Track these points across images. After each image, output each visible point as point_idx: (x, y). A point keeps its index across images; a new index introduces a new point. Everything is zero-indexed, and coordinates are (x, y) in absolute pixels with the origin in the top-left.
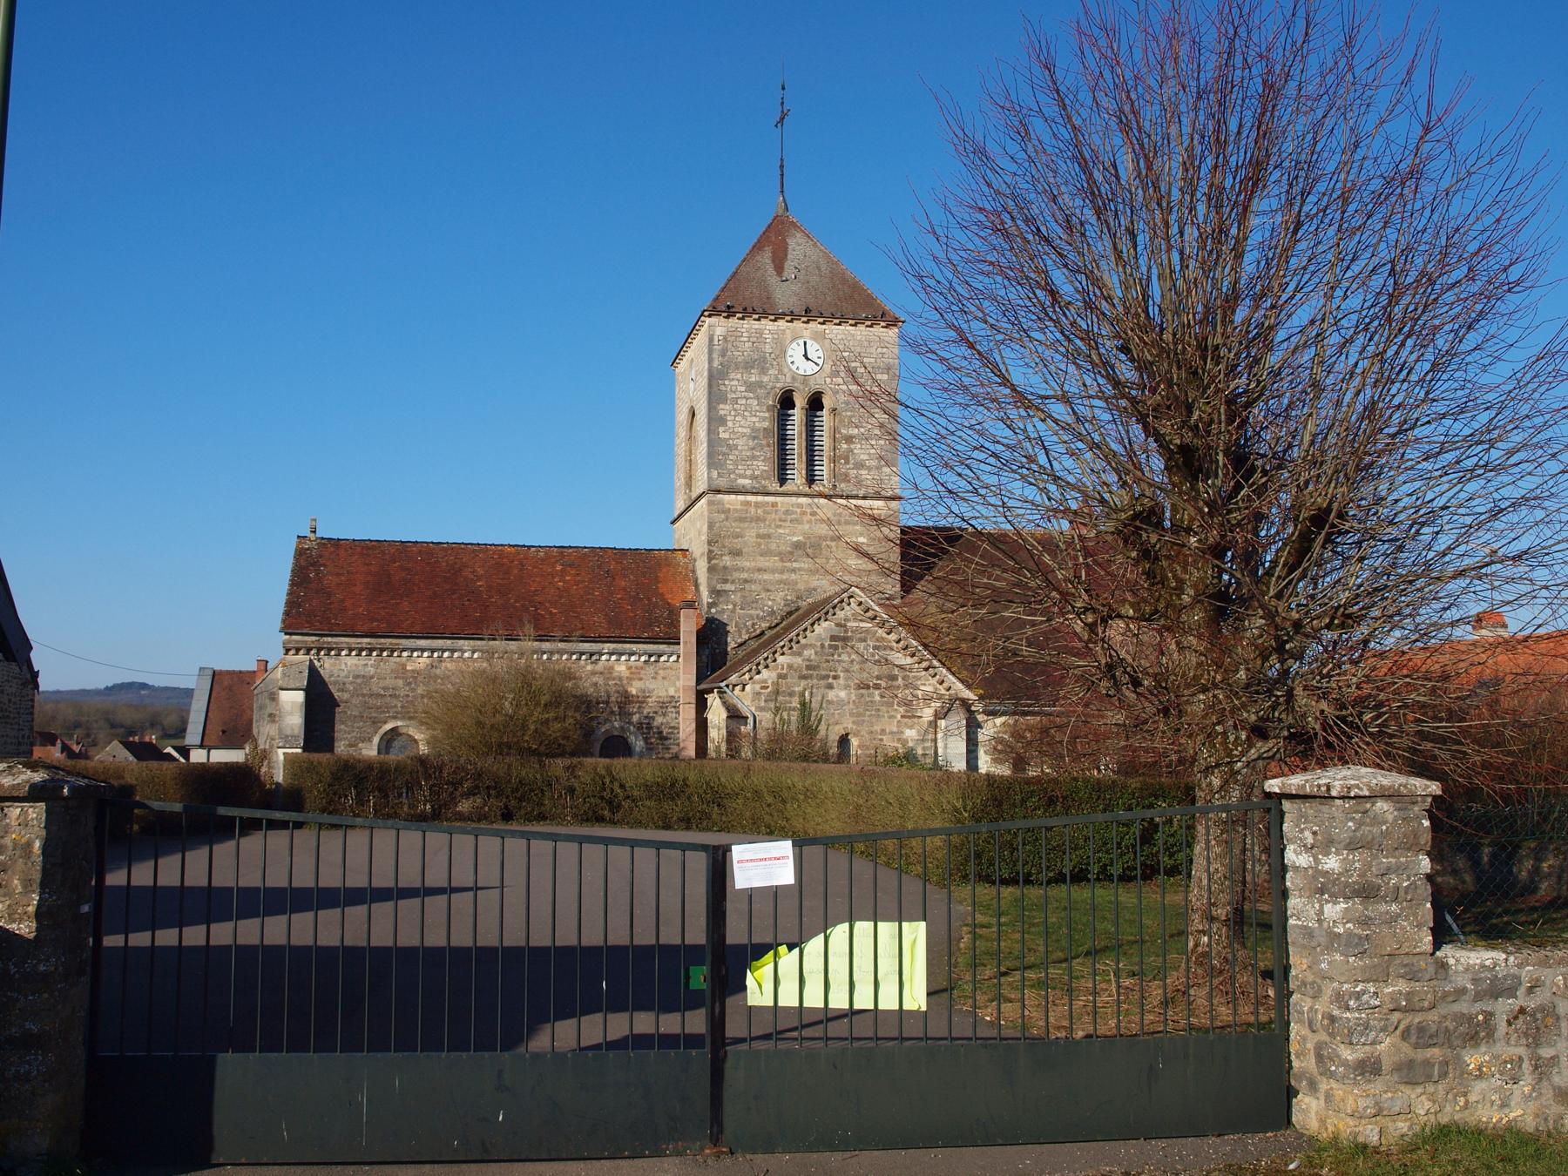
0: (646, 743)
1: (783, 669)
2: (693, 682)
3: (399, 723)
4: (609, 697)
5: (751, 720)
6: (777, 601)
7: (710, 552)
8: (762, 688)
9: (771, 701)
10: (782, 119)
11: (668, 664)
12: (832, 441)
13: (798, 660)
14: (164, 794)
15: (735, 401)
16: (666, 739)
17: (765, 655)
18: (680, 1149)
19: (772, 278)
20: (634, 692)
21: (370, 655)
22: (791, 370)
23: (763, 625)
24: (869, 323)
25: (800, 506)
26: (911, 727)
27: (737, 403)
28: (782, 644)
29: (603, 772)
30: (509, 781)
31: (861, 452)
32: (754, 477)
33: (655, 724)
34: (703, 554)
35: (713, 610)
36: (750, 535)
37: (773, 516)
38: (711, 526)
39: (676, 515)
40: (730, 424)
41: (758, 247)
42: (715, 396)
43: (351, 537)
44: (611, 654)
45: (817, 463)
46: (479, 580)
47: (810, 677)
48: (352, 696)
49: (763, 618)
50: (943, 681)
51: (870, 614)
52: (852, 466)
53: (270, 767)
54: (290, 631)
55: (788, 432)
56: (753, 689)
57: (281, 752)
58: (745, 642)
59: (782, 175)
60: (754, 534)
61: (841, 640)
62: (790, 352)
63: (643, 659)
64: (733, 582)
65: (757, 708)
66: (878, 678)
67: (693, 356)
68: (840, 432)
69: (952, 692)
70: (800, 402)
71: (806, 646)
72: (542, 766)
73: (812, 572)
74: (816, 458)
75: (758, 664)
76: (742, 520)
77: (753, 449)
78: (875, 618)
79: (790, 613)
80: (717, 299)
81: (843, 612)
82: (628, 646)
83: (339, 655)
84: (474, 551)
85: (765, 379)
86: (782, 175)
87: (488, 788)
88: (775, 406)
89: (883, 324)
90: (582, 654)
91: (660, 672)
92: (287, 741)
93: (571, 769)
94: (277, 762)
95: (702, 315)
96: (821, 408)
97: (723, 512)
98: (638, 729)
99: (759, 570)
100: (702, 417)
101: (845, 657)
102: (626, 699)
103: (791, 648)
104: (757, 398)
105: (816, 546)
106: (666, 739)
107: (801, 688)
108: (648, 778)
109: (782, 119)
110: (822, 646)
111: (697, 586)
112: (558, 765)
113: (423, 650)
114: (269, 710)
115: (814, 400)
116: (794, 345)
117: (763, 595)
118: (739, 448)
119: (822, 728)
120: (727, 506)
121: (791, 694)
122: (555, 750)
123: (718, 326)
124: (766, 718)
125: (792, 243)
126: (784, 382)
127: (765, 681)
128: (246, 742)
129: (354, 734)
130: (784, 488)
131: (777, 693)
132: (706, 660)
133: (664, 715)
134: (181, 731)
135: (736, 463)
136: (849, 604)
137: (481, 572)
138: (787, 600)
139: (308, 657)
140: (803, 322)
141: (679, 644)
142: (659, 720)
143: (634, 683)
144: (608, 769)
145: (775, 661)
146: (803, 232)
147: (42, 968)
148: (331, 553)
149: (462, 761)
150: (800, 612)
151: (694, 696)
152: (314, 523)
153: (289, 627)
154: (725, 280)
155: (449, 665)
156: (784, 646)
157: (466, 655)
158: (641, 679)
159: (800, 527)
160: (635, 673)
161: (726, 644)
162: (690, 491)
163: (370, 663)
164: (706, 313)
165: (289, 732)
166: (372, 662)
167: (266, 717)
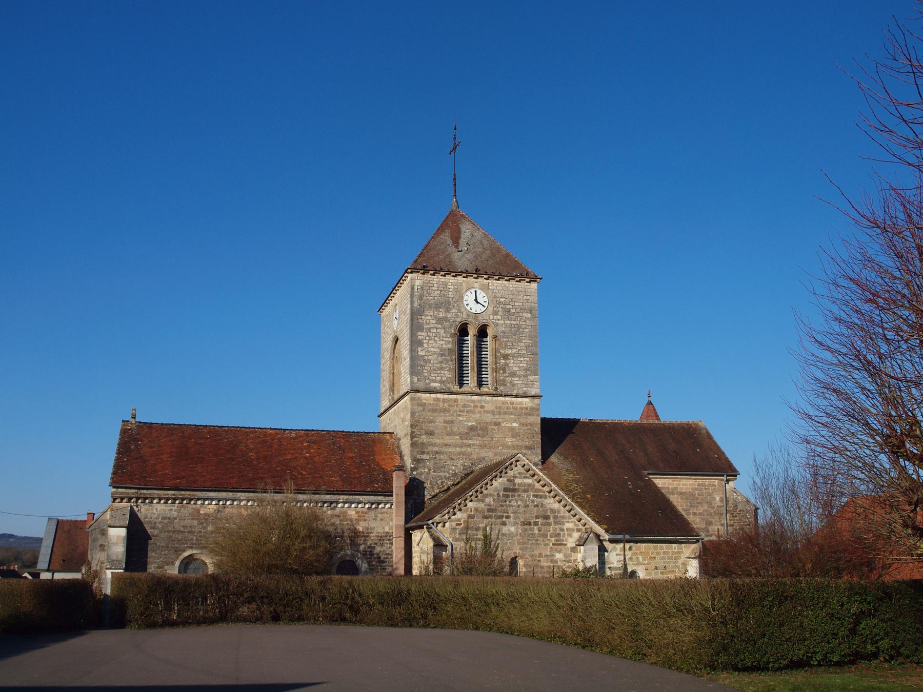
1: (471, 511)
2: (403, 522)
3: (195, 552)
4: (343, 533)
5: (449, 548)
6: (458, 466)
7: (412, 432)
8: (457, 525)
9: (464, 534)
10: (455, 148)
11: (384, 510)
12: (494, 358)
13: (481, 505)
14: (21, 603)
19: (452, 250)
20: (361, 529)
22: (466, 309)
23: (449, 483)
24: (518, 279)
25: (473, 401)
26: (560, 552)
27: (430, 332)
28: (470, 493)
29: (346, 585)
30: (278, 593)
31: (513, 365)
32: (442, 382)
33: (376, 552)
34: (407, 434)
35: (415, 473)
36: (440, 420)
37: (455, 408)
38: (413, 415)
39: (382, 411)
40: (425, 345)
41: (441, 229)
42: (415, 326)
43: (160, 422)
44: (345, 503)
45: (483, 373)
46: (251, 451)
47: (490, 517)
48: (161, 532)
49: (449, 478)
50: (581, 519)
51: (531, 472)
53: (100, 583)
54: (116, 485)
55: (465, 352)
59: (455, 185)
60: (442, 421)
61: (511, 490)
62: (465, 298)
63: (367, 506)
64: (428, 453)
66: (537, 517)
67: (396, 301)
68: (499, 352)
69: (586, 526)
70: (472, 331)
71: (487, 495)
72: (302, 582)
73: (482, 446)
75: (454, 508)
76: (434, 411)
77: (441, 362)
79: (467, 475)
80: (416, 261)
81: (512, 471)
82: (356, 497)
83: (152, 503)
84: (246, 432)
85: (449, 315)
86: (455, 185)
87: (262, 597)
88: (456, 334)
89: (528, 280)
90: (324, 502)
91: (379, 515)
92: (113, 564)
93: (323, 583)
94: (106, 579)
95: (406, 272)
96: (486, 336)
97: (421, 405)
98: (364, 555)
99: (446, 445)
100: (405, 342)
101: (513, 503)
102: (355, 534)
103: (477, 497)
104: (444, 328)
106: (383, 562)
107: (484, 525)
108: (380, 589)
109: (455, 148)
111: (401, 456)
112: (313, 581)
113: (212, 500)
114: (100, 542)
115: (481, 330)
119: (499, 553)
120: (424, 401)
121: (477, 529)
122: (309, 569)
123: (418, 279)
124: (460, 546)
127: (459, 520)
128: (82, 565)
129: (162, 559)
130: (462, 390)
131: (467, 528)
132: (410, 507)
133: (382, 545)
134: (35, 563)
135: (429, 372)
136: (516, 466)
137: (252, 446)
138: (465, 466)
139: (129, 504)
140: (475, 278)
141: (392, 496)
142: (378, 549)
143: (360, 523)
151: (403, 532)
152: (134, 412)
153: (115, 483)
156: (472, 495)
157: (243, 503)
158: (365, 520)
160: (361, 516)
161: (424, 496)
162: (393, 393)
163: (174, 508)
164: (409, 271)
165: (114, 557)
166: (175, 508)
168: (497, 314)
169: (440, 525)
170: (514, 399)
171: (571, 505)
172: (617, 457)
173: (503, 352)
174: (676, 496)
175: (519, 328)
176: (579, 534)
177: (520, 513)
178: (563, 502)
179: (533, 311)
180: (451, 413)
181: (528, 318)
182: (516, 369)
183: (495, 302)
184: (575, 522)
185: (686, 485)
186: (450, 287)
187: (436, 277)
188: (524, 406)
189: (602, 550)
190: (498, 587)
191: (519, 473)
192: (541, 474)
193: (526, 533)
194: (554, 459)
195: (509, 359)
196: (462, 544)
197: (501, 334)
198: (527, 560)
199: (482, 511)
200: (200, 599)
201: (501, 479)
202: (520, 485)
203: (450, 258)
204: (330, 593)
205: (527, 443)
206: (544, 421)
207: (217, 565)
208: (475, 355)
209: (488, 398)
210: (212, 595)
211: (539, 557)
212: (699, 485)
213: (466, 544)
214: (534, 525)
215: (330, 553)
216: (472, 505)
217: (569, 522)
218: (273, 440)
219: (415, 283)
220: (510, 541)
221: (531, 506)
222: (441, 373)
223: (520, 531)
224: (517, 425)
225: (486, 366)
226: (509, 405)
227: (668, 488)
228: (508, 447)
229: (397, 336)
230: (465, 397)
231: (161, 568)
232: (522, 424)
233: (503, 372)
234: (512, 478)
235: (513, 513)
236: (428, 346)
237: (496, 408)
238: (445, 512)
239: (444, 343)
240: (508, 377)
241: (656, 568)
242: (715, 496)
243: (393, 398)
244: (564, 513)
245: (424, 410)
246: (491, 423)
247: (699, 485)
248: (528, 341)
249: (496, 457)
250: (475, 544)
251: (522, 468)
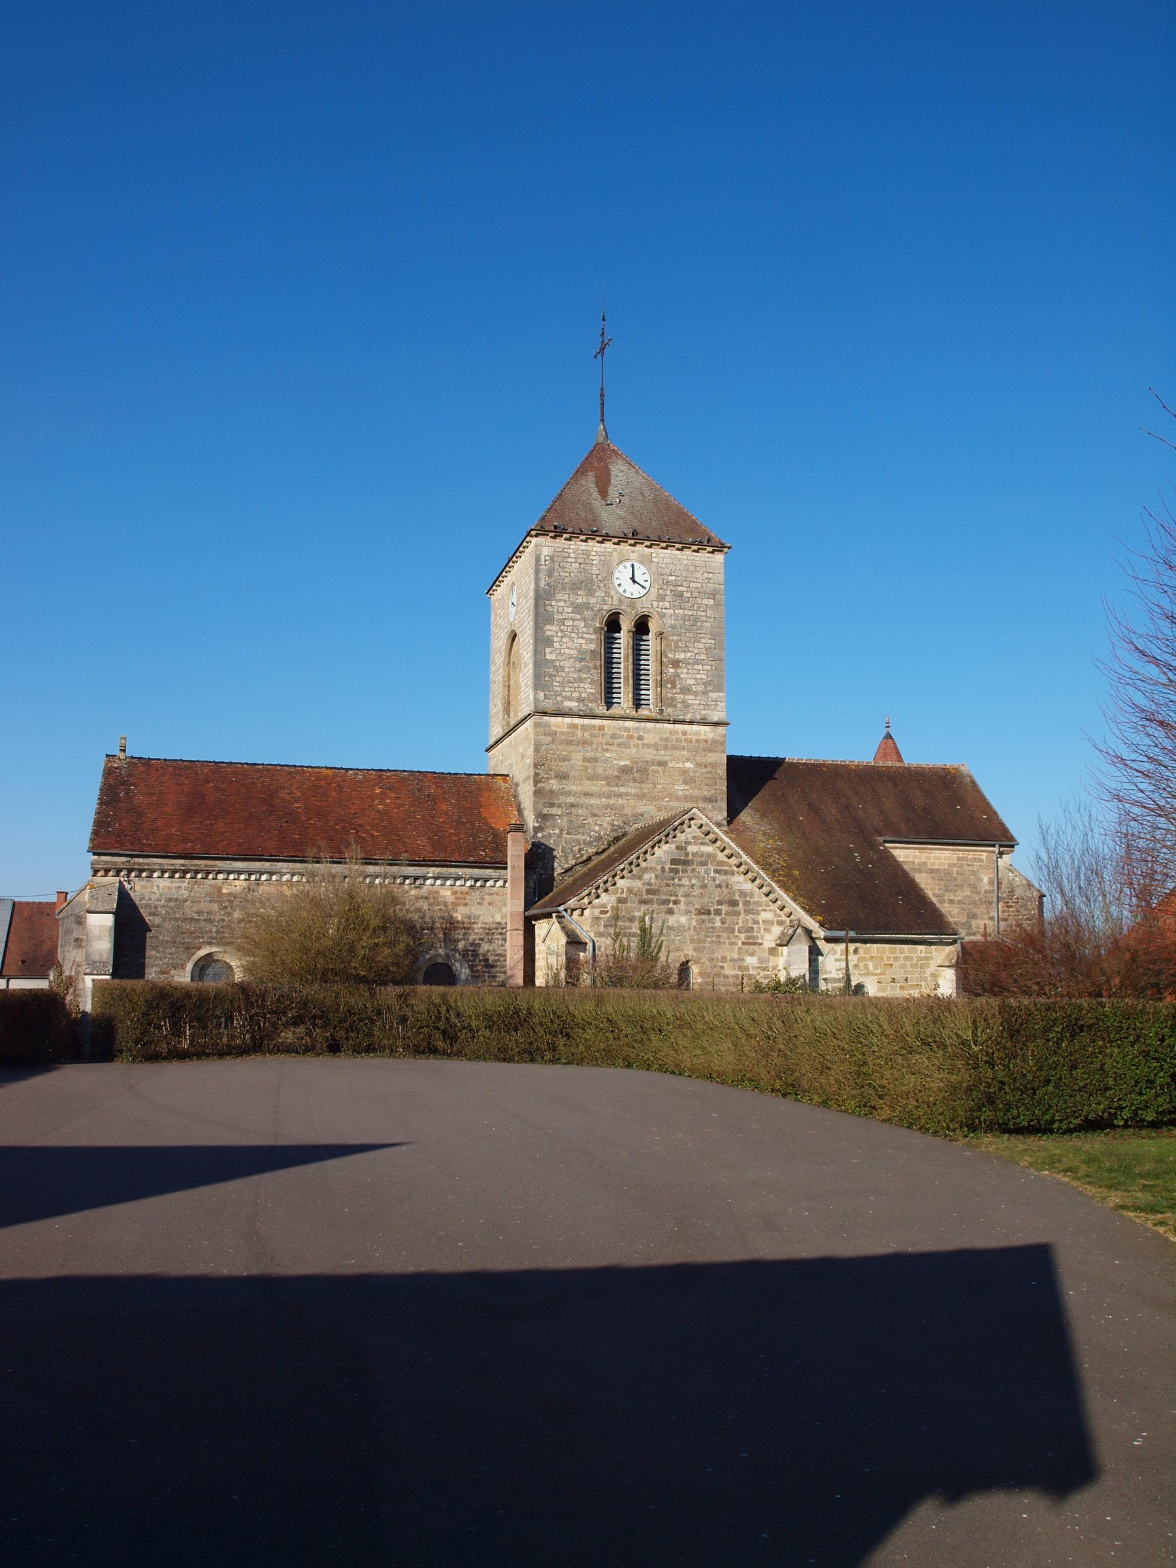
0: (472, 971)
1: (622, 893)
3: (214, 949)
4: (433, 922)
5: (590, 947)
6: (604, 826)
7: (536, 775)
8: (602, 912)
9: (611, 926)
10: (603, 349)
12: (658, 665)
13: (637, 884)
16: (493, 966)
17: (605, 878)
20: (459, 918)
21: (184, 877)
22: (617, 592)
23: (590, 850)
24: (695, 548)
25: (627, 729)
26: (752, 954)
27: (564, 625)
28: (622, 866)
29: (438, 1001)
30: (337, 1011)
31: (687, 677)
32: (580, 700)
33: (481, 951)
35: (540, 835)
37: (600, 739)
38: (537, 748)
39: (491, 742)
40: (556, 645)
41: (581, 471)
42: (541, 617)
44: (436, 878)
45: (642, 687)
49: (590, 844)
51: (711, 836)
52: (679, 691)
54: (98, 851)
56: (592, 913)
57: (88, 980)
58: (572, 868)
59: (602, 404)
61: (681, 863)
62: (616, 575)
63: (469, 883)
64: (559, 806)
66: (719, 903)
69: (792, 917)
70: (627, 625)
71: (646, 870)
72: (373, 994)
73: (640, 797)
74: (642, 682)
76: (569, 743)
77: (580, 671)
78: (715, 841)
79: (617, 839)
80: (543, 518)
82: (453, 870)
85: (592, 601)
86: (602, 404)
87: (314, 1017)
88: (602, 628)
89: (710, 549)
90: (406, 878)
91: (486, 897)
92: (95, 967)
94: (84, 989)
95: (528, 535)
96: (647, 632)
98: (464, 956)
99: (586, 794)
101: (685, 881)
102: (451, 926)
103: (631, 871)
104: (584, 619)
105: (644, 771)
107: (641, 913)
108: (488, 1006)
109: (603, 349)
110: (663, 869)
111: (520, 811)
112: (389, 994)
113: (240, 873)
114: (75, 935)
116: (621, 567)
117: (590, 820)
118: (566, 669)
120: (554, 728)
121: (631, 920)
123: (545, 546)
124: (605, 945)
126: (611, 604)
127: (604, 906)
130: (611, 712)
131: (616, 918)
133: (491, 941)
135: (562, 685)
136: (690, 826)
137: (298, 794)
138: (613, 825)
139: (118, 878)
140: (630, 545)
142: (485, 947)
143: (459, 908)
144: (444, 997)
145: (615, 884)
146: (624, 459)
148: (142, 772)
149: (286, 988)
150: (629, 837)
152: (123, 741)
153: (97, 848)
154: (550, 502)
156: (623, 869)
157: (285, 878)
158: (466, 905)
159: (627, 751)
160: (461, 899)
161: (553, 869)
163: (183, 885)
164: (533, 533)
165: (96, 958)
166: (186, 884)
167: (72, 941)
168: (663, 600)
169: (576, 913)
170: (687, 727)
171: (769, 885)
173: (672, 656)
174: (924, 875)
176: (781, 928)
177: (694, 896)
178: (758, 882)
179: (717, 596)
180: (594, 746)
181: (710, 607)
184: (775, 911)
185: (939, 858)
186: (594, 558)
187: (572, 543)
188: (702, 737)
190: (663, 1005)
191: (694, 838)
192: (727, 840)
196: (609, 941)
197: (670, 629)
198: (704, 966)
200: (223, 1020)
201: (667, 845)
203: (594, 514)
205: (706, 793)
206: (731, 760)
207: (248, 969)
209: (649, 725)
210: (240, 1014)
211: (721, 962)
212: (958, 859)
213: (615, 941)
215: (413, 953)
216: (624, 884)
217: (766, 910)
220: (679, 938)
221: (711, 886)
222: (579, 687)
223: (695, 923)
224: (692, 766)
226: (680, 736)
227: (914, 862)
228: (678, 799)
230: (614, 722)
233: (672, 687)
234: (683, 845)
235: (684, 896)
236: (561, 645)
239: (584, 641)
240: (680, 693)
241: (893, 981)
242: (982, 876)
243: (508, 723)
244: (759, 897)
245: (553, 741)
246: (653, 761)
247: (958, 859)
248: (710, 641)
250: (629, 941)
251: (698, 830)
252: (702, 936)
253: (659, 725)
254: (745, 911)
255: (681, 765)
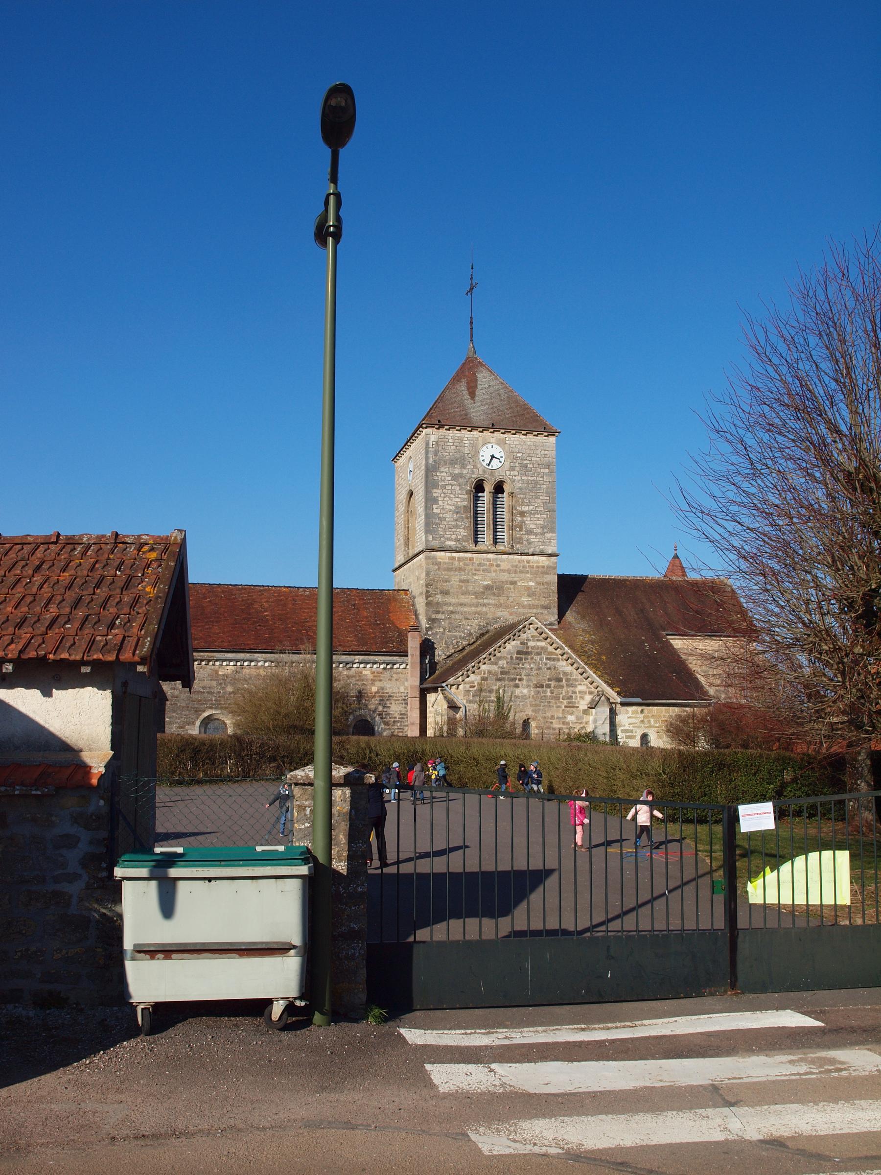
1: (485, 674)
6: (473, 626)
7: (427, 592)
8: (471, 687)
9: (477, 696)
10: (471, 289)
12: (510, 515)
13: (495, 668)
15: (444, 487)
17: (473, 664)
18: (713, 992)
19: (468, 402)
23: (464, 643)
25: (489, 560)
26: (571, 714)
28: (484, 656)
29: (363, 746)
30: (299, 752)
31: (530, 523)
32: (457, 540)
34: (421, 593)
35: (430, 633)
36: (455, 579)
37: (471, 567)
38: (428, 574)
39: (396, 566)
40: (440, 503)
41: (457, 378)
42: (430, 484)
44: (360, 663)
46: (266, 611)
49: (464, 638)
51: (544, 635)
56: (465, 687)
59: (472, 329)
61: (523, 653)
62: (481, 453)
63: (382, 666)
64: (443, 613)
65: (467, 701)
66: (550, 680)
69: (599, 689)
70: (489, 487)
71: (500, 658)
73: (498, 606)
76: (449, 570)
77: (456, 520)
79: (482, 635)
82: (372, 657)
84: (260, 591)
85: (465, 472)
86: (472, 329)
87: (283, 757)
88: (471, 491)
89: (546, 434)
96: (502, 492)
97: (436, 564)
99: (461, 605)
101: (526, 666)
103: (490, 659)
104: (459, 485)
105: (500, 588)
109: (471, 289)
110: (512, 658)
111: (416, 615)
113: (230, 661)
117: (464, 622)
118: (447, 519)
119: (511, 715)
120: (439, 560)
121: (491, 691)
123: (431, 435)
124: (473, 708)
125: (480, 376)
126: (478, 474)
131: (481, 690)
135: (445, 530)
138: (480, 625)
140: (491, 432)
141: (407, 656)
144: (368, 745)
145: (479, 668)
147: (360, 890)
151: (418, 692)
155: (247, 671)
157: (260, 664)
158: (381, 680)
159: (489, 575)
160: (377, 677)
162: (408, 548)
164: (424, 426)
168: (514, 470)
171: (583, 668)
172: (636, 617)
175: (536, 484)
176: (591, 696)
178: (575, 665)
179: (551, 467)
182: (532, 526)
183: (512, 457)
188: (541, 564)
189: (613, 713)
191: (532, 636)
192: (554, 637)
193: (539, 695)
194: (570, 616)
195: (525, 516)
196: (476, 706)
199: (495, 674)
202: (532, 648)
204: (348, 753)
205: (543, 603)
206: (562, 578)
207: (237, 725)
208: (491, 512)
209: (504, 557)
213: (480, 706)
214: (547, 687)
218: (287, 599)
219: (429, 438)
224: (533, 584)
225: (502, 523)
228: (524, 607)
229: (411, 490)
231: (182, 728)
232: (538, 583)
237: (512, 566)
238: (459, 674)
239: (459, 500)
243: (408, 553)
244: (576, 675)
245: (439, 569)
249: (511, 617)
250: (489, 705)
252: (538, 702)
253: (511, 557)
254: (567, 685)
255: (526, 584)
